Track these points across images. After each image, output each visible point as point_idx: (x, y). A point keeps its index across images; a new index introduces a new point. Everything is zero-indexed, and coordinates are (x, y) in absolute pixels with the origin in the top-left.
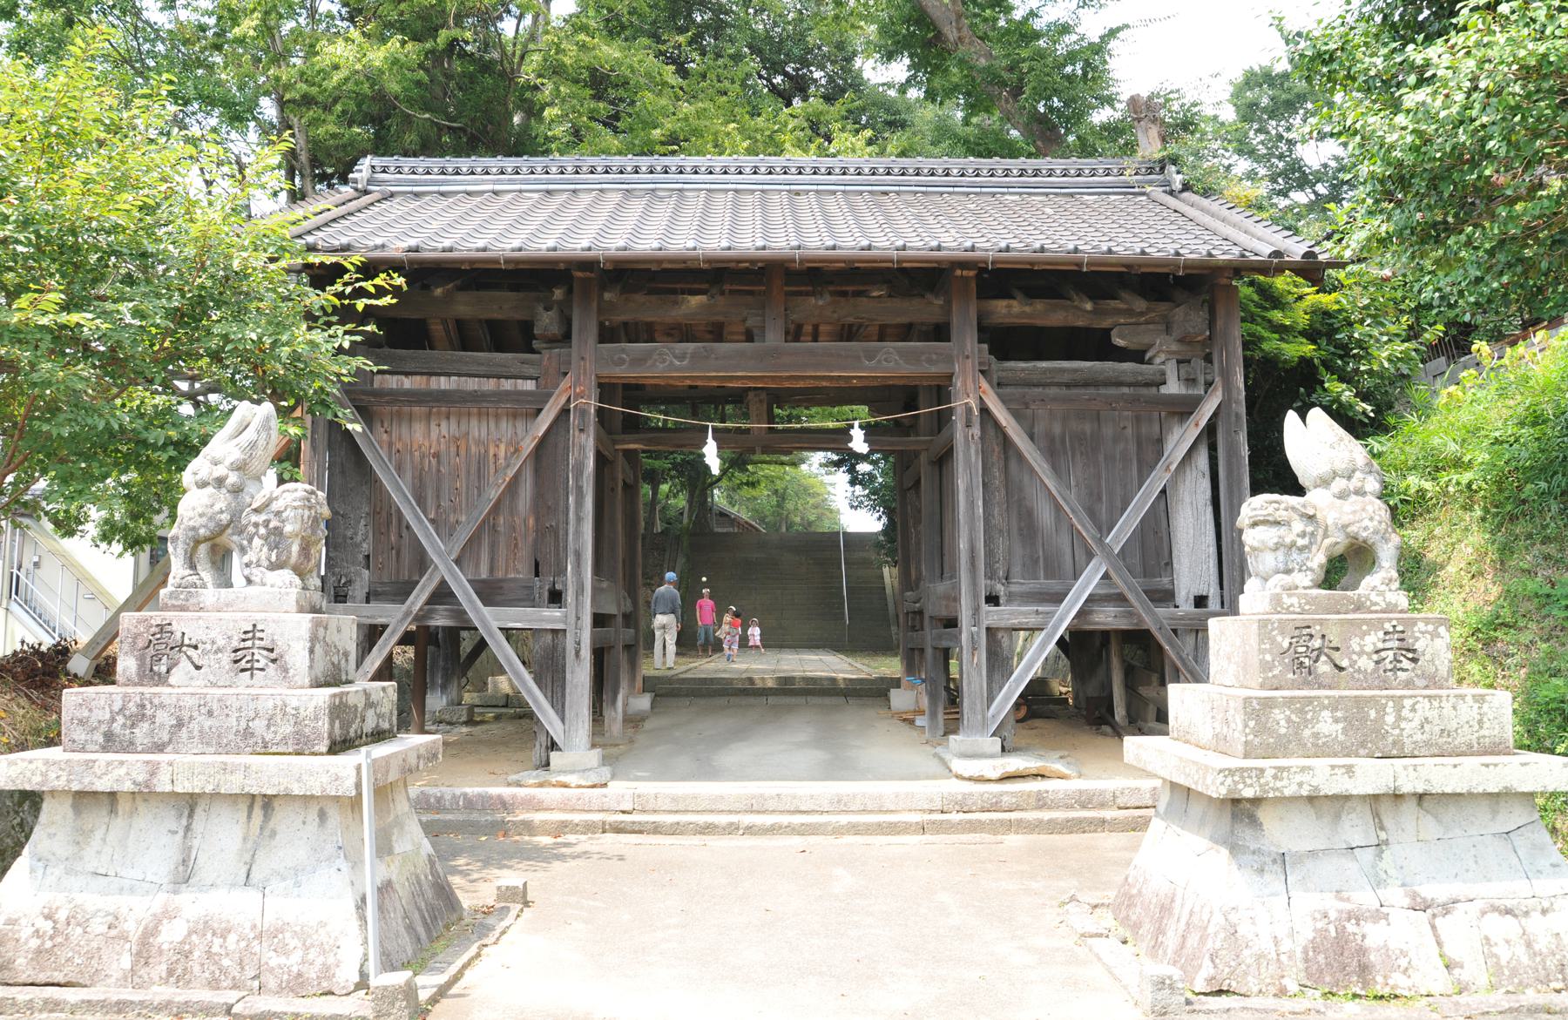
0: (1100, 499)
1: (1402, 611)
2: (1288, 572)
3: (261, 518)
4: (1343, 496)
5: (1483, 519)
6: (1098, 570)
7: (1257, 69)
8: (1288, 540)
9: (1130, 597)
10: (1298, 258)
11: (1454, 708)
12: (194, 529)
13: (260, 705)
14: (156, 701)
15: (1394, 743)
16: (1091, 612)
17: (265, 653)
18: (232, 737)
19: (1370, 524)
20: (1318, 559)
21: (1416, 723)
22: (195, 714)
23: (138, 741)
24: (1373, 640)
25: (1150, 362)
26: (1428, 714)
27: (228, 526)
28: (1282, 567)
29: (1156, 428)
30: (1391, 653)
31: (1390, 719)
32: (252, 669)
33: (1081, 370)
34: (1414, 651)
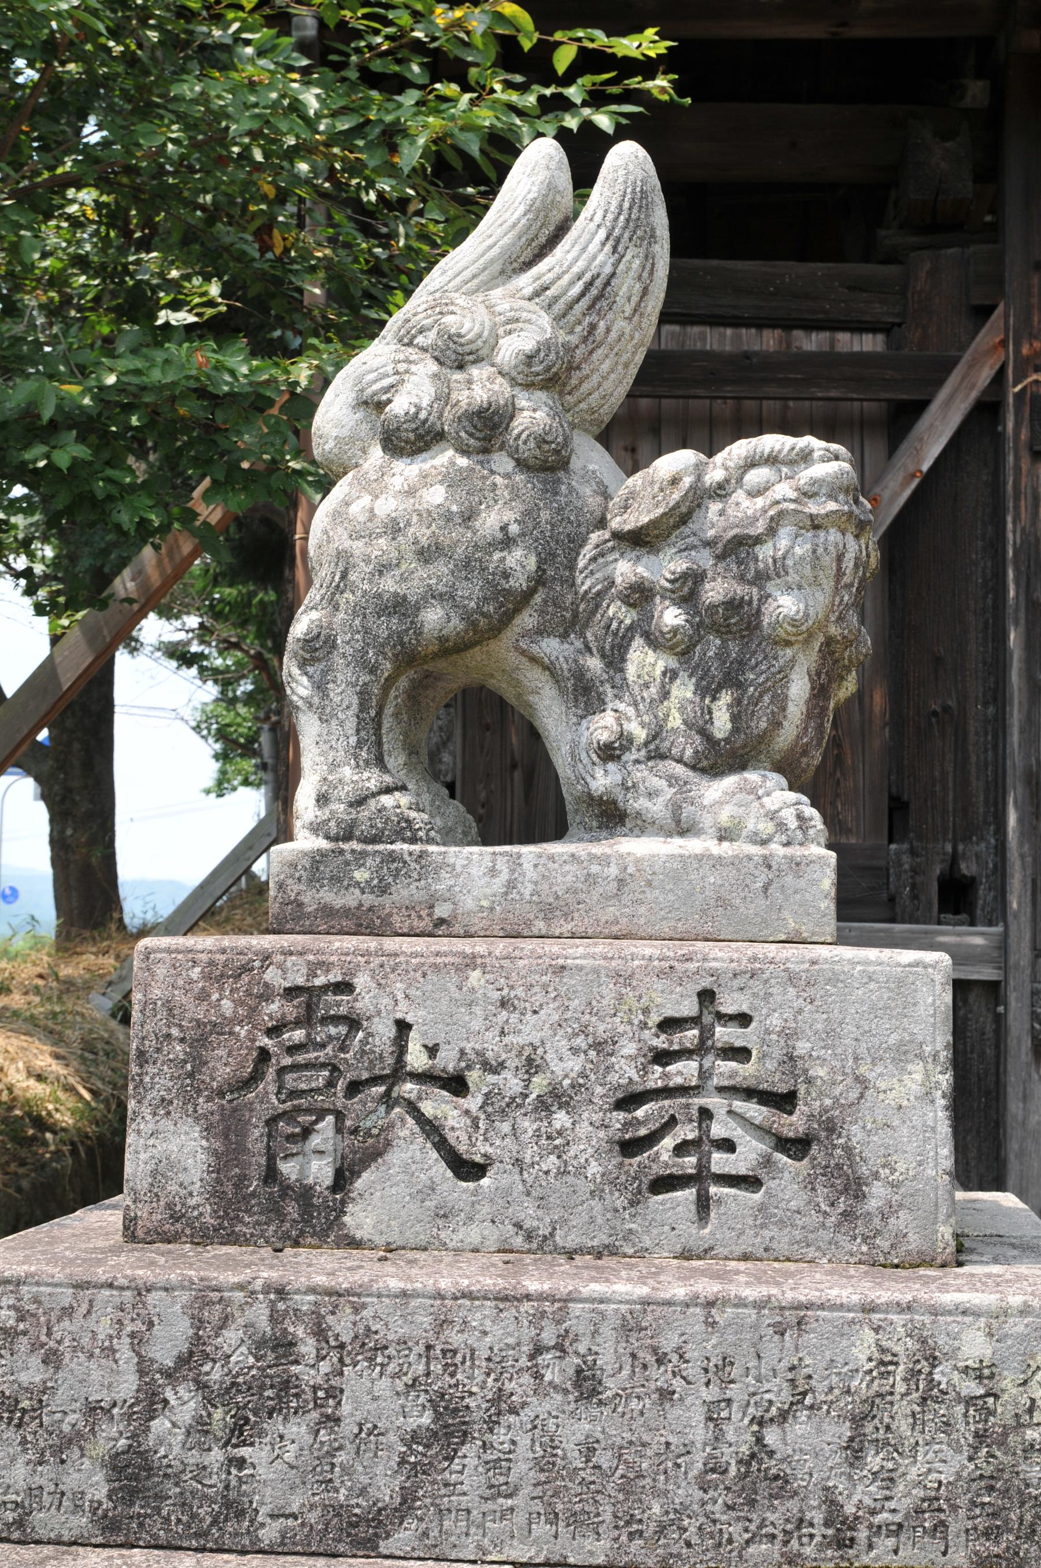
3: (666, 566)
12: (398, 606)
13: (813, 1352)
14: (342, 1325)
17: (755, 1111)
18: (686, 1492)
22: (519, 1386)
23: (265, 1499)
27: (527, 596)
32: (700, 1178)
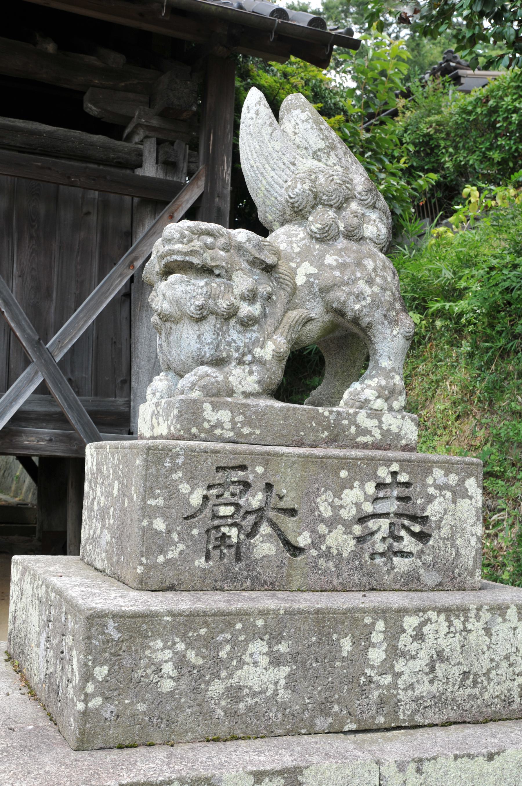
0: (49, 296)
1: (407, 448)
2: (219, 362)
4: (325, 237)
5: (471, 355)
6: (31, 381)
7: (296, 4)
8: (223, 304)
9: (70, 416)
10: (305, 24)
11: (488, 631)
15: (382, 702)
16: (19, 433)
19: (368, 290)
20: (273, 347)
21: (421, 663)
24: (355, 497)
25: (128, 139)
26: (443, 643)
28: (208, 352)
29: (126, 220)
30: (384, 523)
31: (377, 655)
33: (39, 133)
34: (424, 520)
